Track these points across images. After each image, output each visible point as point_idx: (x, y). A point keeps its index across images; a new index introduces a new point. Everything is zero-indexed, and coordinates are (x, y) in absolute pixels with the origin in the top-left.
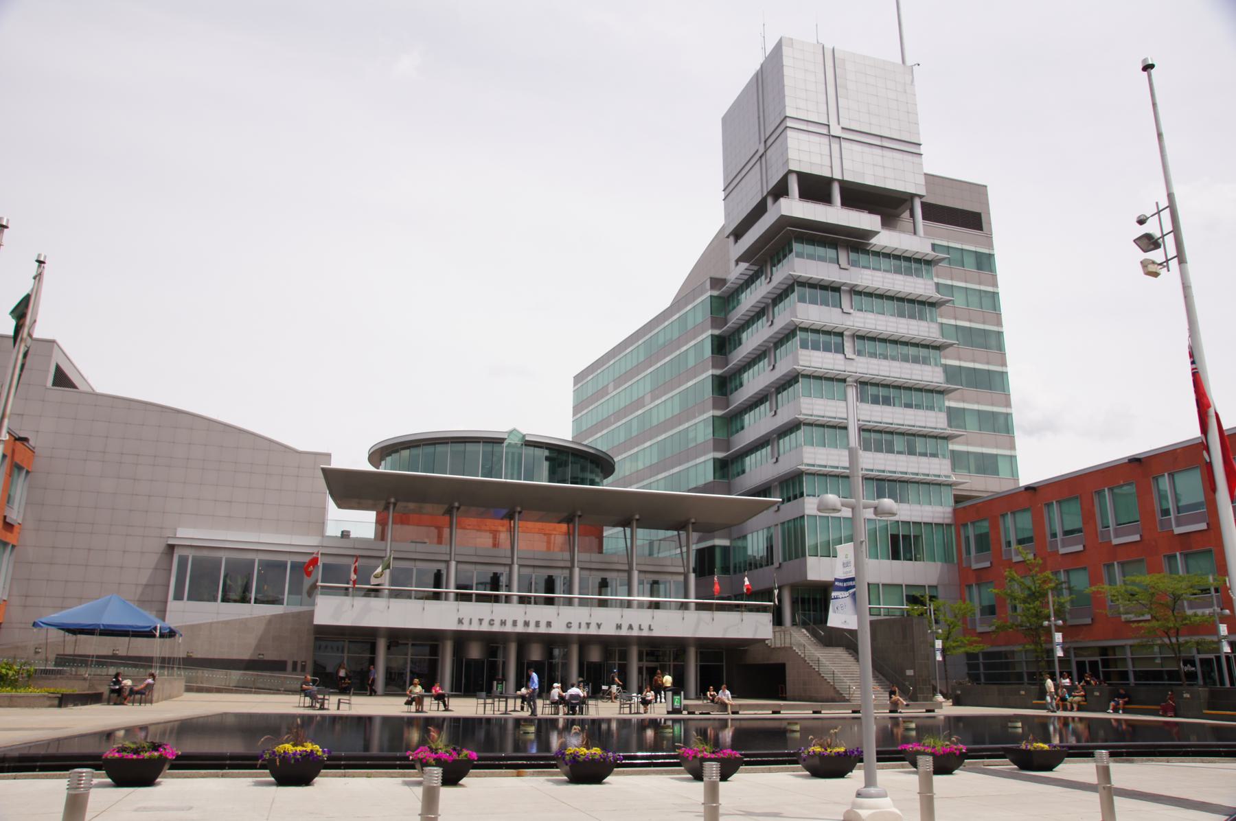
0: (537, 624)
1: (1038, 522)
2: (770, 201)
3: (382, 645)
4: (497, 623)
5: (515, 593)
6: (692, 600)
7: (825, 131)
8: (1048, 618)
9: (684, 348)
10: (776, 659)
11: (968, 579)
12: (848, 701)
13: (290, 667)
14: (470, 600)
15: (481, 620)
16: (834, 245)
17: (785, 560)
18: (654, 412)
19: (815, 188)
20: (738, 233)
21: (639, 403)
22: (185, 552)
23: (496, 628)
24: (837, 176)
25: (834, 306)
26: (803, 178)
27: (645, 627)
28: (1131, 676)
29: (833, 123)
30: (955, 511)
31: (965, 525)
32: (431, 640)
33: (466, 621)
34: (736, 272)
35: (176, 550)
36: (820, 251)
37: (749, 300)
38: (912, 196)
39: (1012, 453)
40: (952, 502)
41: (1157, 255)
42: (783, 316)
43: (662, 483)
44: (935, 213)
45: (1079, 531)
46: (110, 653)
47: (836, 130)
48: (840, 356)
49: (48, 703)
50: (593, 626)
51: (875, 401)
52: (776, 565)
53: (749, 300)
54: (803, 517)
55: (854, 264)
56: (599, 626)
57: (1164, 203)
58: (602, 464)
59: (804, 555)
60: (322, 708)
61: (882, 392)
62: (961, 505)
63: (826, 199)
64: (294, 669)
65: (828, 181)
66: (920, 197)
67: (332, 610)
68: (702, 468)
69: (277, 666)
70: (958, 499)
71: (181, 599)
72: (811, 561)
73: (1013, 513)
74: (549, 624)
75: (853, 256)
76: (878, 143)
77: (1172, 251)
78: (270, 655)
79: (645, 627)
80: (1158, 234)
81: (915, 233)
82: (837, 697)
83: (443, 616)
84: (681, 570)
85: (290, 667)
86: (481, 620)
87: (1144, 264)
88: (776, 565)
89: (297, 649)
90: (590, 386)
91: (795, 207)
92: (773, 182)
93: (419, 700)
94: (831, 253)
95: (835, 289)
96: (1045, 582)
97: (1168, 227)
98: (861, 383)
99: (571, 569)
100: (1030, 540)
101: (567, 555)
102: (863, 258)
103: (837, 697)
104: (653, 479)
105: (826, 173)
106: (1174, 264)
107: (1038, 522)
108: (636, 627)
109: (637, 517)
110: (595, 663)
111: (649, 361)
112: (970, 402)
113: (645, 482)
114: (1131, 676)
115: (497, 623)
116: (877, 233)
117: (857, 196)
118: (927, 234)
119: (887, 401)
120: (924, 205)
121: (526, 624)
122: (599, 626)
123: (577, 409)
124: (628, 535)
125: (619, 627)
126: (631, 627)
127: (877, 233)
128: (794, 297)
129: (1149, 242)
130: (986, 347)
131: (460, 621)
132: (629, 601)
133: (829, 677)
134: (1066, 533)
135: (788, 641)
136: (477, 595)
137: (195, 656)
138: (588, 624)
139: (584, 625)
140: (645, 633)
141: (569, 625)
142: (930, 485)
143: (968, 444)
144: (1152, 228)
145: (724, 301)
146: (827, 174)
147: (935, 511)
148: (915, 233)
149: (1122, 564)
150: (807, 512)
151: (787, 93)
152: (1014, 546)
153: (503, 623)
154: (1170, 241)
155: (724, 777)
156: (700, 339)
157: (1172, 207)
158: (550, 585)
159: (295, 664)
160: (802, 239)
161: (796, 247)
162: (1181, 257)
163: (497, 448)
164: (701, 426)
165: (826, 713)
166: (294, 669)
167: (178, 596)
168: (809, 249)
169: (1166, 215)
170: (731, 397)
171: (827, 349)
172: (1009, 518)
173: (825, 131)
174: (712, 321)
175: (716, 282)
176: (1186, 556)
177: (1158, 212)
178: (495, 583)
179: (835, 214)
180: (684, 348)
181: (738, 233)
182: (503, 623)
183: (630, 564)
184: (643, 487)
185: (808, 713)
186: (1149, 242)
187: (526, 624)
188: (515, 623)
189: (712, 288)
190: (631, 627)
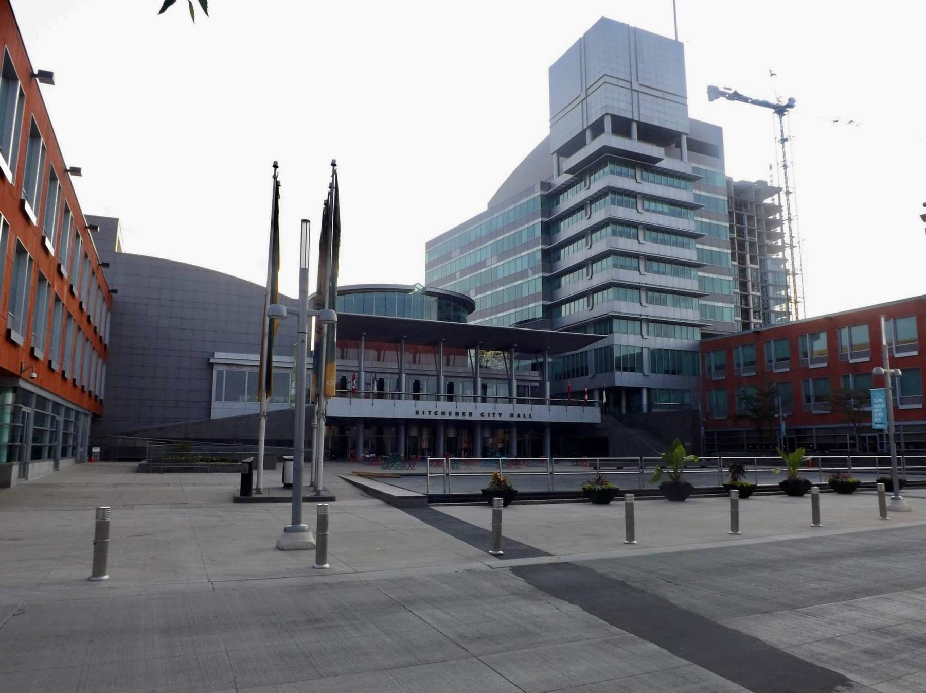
0: (464, 414)
2: (588, 134)
3: (548, 431)
8: (778, 413)
9: (520, 229)
15: (430, 412)
16: (633, 166)
17: (596, 373)
18: (500, 269)
19: (622, 126)
20: (567, 150)
21: (482, 264)
22: (221, 368)
23: (432, 417)
24: (636, 118)
25: (633, 208)
26: (615, 118)
27: (527, 415)
31: (708, 352)
32: (539, 427)
35: (215, 367)
36: (625, 170)
37: (568, 201)
42: (599, 214)
45: (786, 359)
46: (183, 436)
47: (636, 86)
50: (497, 415)
52: (590, 375)
53: (568, 201)
56: (500, 415)
58: (467, 305)
59: (612, 370)
63: (627, 134)
66: (687, 134)
68: (535, 309)
70: (703, 335)
71: (221, 400)
73: (743, 346)
74: (470, 414)
81: (682, 160)
83: (403, 409)
86: (430, 412)
88: (590, 375)
90: (439, 250)
92: (593, 120)
94: (631, 171)
100: (752, 363)
101: (395, 365)
105: (629, 116)
107: (760, 353)
108: (522, 416)
111: (491, 236)
118: (691, 160)
120: (689, 140)
121: (457, 414)
122: (500, 415)
123: (429, 266)
125: (512, 415)
128: (608, 198)
131: (417, 413)
138: (494, 414)
145: (551, 197)
146: (629, 116)
148: (682, 160)
149: (814, 380)
150: (616, 343)
152: (742, 367)
153: (443, 413)
155: (505, 505)
156: (532, 223)
160: (614, 161)
164: (534, 282)
167: (219, 398)
171: (629, 237)
173: (628, 85)
174: (542, 211)
175: (545, 185)
176: (855, 376)
179: (634, 145)
180: (520, 229)
183: (400, 369)
188: (450, 414)
189: (542, 189)
190: (519, 416)
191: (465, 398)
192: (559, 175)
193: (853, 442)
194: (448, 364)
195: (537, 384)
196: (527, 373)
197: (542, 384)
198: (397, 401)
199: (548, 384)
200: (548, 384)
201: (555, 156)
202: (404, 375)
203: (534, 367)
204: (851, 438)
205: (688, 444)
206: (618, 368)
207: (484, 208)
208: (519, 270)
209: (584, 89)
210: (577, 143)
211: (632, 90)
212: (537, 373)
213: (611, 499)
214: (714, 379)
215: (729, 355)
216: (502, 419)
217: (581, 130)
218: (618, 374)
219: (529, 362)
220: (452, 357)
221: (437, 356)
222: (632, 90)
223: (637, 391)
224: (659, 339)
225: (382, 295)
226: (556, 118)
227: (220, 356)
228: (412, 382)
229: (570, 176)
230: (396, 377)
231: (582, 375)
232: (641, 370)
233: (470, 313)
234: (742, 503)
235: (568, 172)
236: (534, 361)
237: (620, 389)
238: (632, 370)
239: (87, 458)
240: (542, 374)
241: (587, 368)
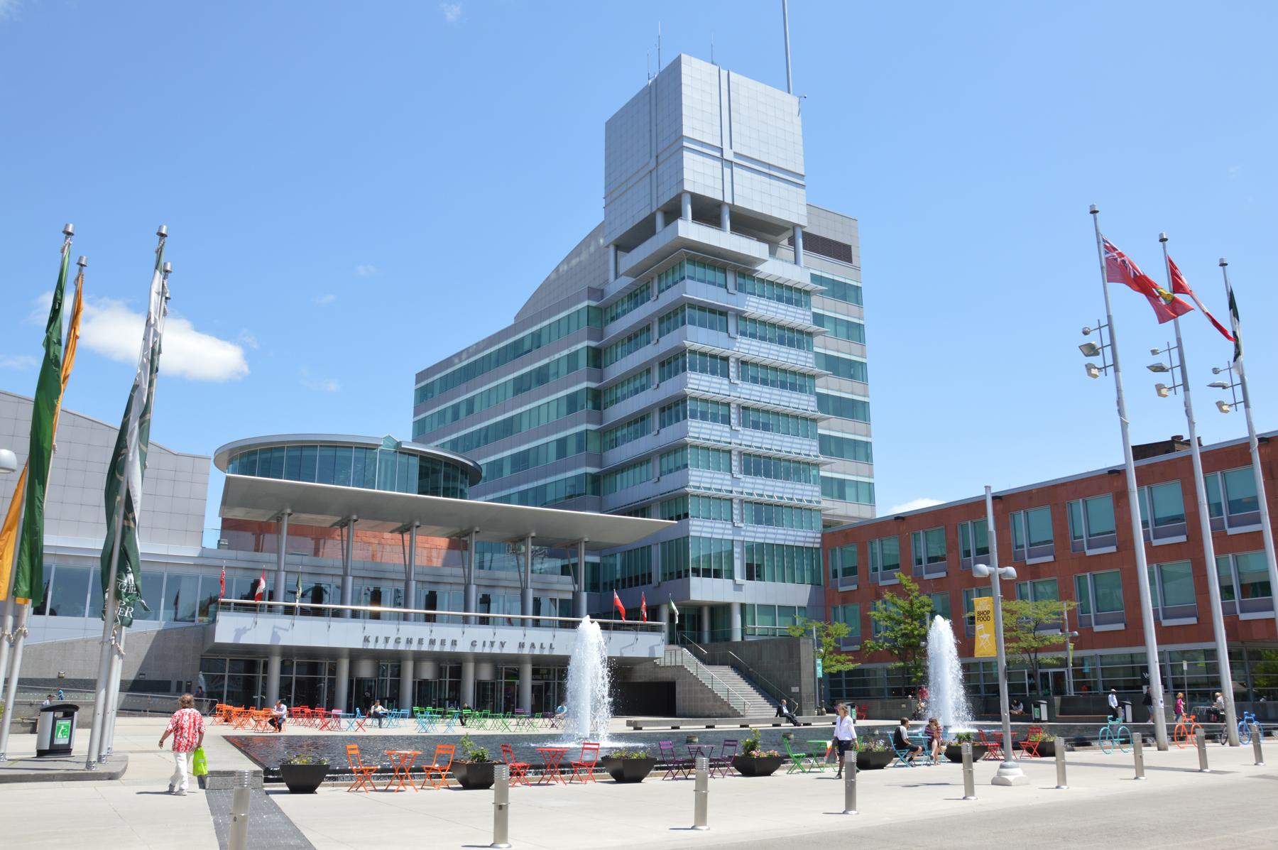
0: (443, 642)
1: (904, 547)
2: (659, 220)
4: (403, 641)
6: (530, 616)
7: (718, 155)
10: (666, 676)
11: (825, 604)
13: (174, 687)
14: (229, 609)
17: (664, 580)
19: (708, 212)
20: (625, 244)
24: (728, 200)
25: (721, 330)
26: (697, 200)
27: (547, 646)
28: (983, 689)
29: (726, 147)
30: (823, 535)
33: (372, 640)
34: (617, 286)
36: (710, 274)
38: (795, 226)
39: (871, 480)
40: (821, 528)
41: (1097, 361)
43: (516, 498)
44: (817, 244)
47: (728, 155)
48: (726, 381)
49: (23, 729)
55: (740, 288)
57: (1104, 322)
62: (829, 530)
65: (718, 205)
67: (231, 629)
72: (695, 581)
74: (454, 643)
75: (740, 280)
76: (766, 171)
77: (1109, 361)
78: (153, 676)
79: (547, 646)
80: (1098, 345)
82: (729, 713)
85: (174, 687)
87: (1089, 367)
89: (184, 667)
91: (689, 230)
92: (665, 199)
93: (276, 722)
94: (720, 276)
95: (723, 313)
96: (923, 606)
97: (1107, 341)
98: (744, 408)
99: (344, 577)
102: (749, 284)
103: (729, 713)
106: (1111, 370)
108: (538, 646)
112: (834, 427)
113: (504, 493)
114: (983, 689)
115: (403, 641)
116: (765, 261)
117: (747, 224)
119: (766, 427)
122: (502, 644)
124: (407, 543)
126: (533, 646)
127: (765, 261)
129: (1091, 350)
130: (852, 377)
131: (366, 640)
132: (523, 620)
133: (723, 695)
134: (931, 560)
135: (679, 659)
137: (67, 676)
138: (492, 644)
139: (488, 644)
141: (473, 644)
142: (800, 512)
143: (832, 471)
144: (1093, 339)
145: (601, 315)
147: (805, 536)
151: (684, 112)
153: (409, 641)
154: (1108, 351)
157: (1110, 325)
161: (688, 269)
162: (1115, 365)
165: (719, 727)
168: (699, 271)
169: (1105, 331)
172: (877, 544)
177: (1100, 328)
179: (724, 239)
181: (625, 244)
182: (409, 641)
183: (345, 568)
184: (493, 500)
186: (1091, 350)
187: (432, 642)
190: (533, 646)
192: (616, 277)
193: (1032, 681)
195: (570, 596)
196: (555, 578)
199: (584, 596)
200: (584, 596)
201: (612, 248)
203: (565, 571)
204: (1030, 676)
206: (696, 572)
207: (512, 322)
209: (654, 154)
210: (645, 230)
211: (722, 159)
212: (569, 579)
214: (841, 589)
215: (862, 551)
216: (506, 651)
217: (646, 213)
218: (695, 581)
219: (558, 563)
222: (722, 159)
223: (725, 608)
224: (761, 529)
226: (611, 198)
227: (480, 463)
229: (631, 280)
230: (338, 581)
231: (644, 584)
232: (731, 576)
234: (863, 775)
235: (627, 274)
237: (698, 608)
238: (717, 574)
239: (238, 514)
241: (650, 575)
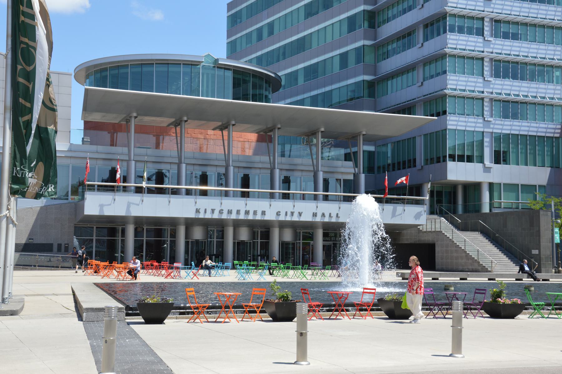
0: (255, 213)
5: (132, 184)
10: (428, 239)
12: (490, 271)
13: (55, 248)
17: (426, 164)
33: (202, 211)
51: (506, 36)
54: (446, 130)
59: (445, 161)
60: (244, 279)
61: (512, 29)
64: (59, 250)
69: (46, 248)
72: (451, 165)
74: (263, 213)
83: (212, 207)
84: (312, 169)
85: (55, 248)
86: (213, 211)
93: (133, 273)
104: (306, 96)
108: (327, 215)
109: (323, 129)
110: (197, 241)
115: (225, 212)
119: (515, 37)
122: (300, 214)
124: (226, 138)
126: (323, 215)
131: (198, 211)
136: (99, 186)
138: (292, 213)
139: (289, 214)
140: (259, 217)
141: (278, 214)
153: (230, 212)
158: (160, 177)
159: (59, 246)
163: (194, 69)
166: (59, 250)
170: (379, 30)
178: (160, 177)
185: (456, 279)
187: (247, 212)
188: (238, 212)
190: (323, 215)
191: (261, 196)
194: (283, 155)
195: (351, 177)
196: (339, 163)
197: (356, 176)
198: (224, 198)
202: (184, 166)
203: (347, 157)
205: (77, 266)
206: (452, 158)
208: (433, 66)
212: (350, 164)
213: (519, 313)
216: (303, 219)
218: (451, 165)
220: (287, 147)
221: (271, 145)
224: (508, 122)
225: (164, 69)
228: (241, 175)
231: (409, 167)
233: (274, 91)
236: (348, 151)
237: (454, 186)
238: (470, 159)
240: (356, 165)
241: (415, 160)
